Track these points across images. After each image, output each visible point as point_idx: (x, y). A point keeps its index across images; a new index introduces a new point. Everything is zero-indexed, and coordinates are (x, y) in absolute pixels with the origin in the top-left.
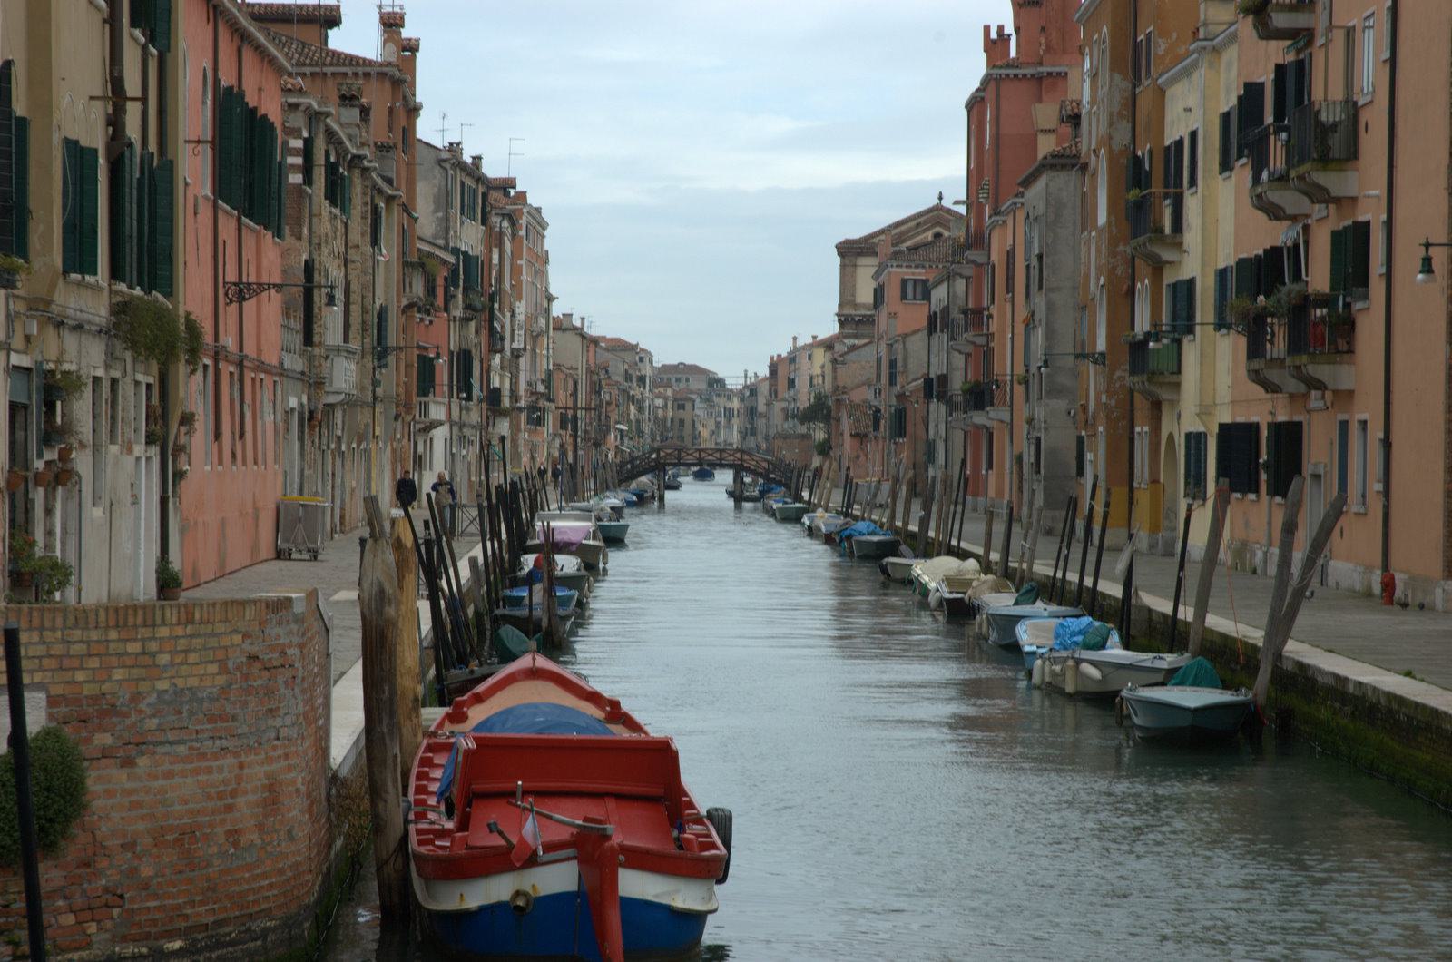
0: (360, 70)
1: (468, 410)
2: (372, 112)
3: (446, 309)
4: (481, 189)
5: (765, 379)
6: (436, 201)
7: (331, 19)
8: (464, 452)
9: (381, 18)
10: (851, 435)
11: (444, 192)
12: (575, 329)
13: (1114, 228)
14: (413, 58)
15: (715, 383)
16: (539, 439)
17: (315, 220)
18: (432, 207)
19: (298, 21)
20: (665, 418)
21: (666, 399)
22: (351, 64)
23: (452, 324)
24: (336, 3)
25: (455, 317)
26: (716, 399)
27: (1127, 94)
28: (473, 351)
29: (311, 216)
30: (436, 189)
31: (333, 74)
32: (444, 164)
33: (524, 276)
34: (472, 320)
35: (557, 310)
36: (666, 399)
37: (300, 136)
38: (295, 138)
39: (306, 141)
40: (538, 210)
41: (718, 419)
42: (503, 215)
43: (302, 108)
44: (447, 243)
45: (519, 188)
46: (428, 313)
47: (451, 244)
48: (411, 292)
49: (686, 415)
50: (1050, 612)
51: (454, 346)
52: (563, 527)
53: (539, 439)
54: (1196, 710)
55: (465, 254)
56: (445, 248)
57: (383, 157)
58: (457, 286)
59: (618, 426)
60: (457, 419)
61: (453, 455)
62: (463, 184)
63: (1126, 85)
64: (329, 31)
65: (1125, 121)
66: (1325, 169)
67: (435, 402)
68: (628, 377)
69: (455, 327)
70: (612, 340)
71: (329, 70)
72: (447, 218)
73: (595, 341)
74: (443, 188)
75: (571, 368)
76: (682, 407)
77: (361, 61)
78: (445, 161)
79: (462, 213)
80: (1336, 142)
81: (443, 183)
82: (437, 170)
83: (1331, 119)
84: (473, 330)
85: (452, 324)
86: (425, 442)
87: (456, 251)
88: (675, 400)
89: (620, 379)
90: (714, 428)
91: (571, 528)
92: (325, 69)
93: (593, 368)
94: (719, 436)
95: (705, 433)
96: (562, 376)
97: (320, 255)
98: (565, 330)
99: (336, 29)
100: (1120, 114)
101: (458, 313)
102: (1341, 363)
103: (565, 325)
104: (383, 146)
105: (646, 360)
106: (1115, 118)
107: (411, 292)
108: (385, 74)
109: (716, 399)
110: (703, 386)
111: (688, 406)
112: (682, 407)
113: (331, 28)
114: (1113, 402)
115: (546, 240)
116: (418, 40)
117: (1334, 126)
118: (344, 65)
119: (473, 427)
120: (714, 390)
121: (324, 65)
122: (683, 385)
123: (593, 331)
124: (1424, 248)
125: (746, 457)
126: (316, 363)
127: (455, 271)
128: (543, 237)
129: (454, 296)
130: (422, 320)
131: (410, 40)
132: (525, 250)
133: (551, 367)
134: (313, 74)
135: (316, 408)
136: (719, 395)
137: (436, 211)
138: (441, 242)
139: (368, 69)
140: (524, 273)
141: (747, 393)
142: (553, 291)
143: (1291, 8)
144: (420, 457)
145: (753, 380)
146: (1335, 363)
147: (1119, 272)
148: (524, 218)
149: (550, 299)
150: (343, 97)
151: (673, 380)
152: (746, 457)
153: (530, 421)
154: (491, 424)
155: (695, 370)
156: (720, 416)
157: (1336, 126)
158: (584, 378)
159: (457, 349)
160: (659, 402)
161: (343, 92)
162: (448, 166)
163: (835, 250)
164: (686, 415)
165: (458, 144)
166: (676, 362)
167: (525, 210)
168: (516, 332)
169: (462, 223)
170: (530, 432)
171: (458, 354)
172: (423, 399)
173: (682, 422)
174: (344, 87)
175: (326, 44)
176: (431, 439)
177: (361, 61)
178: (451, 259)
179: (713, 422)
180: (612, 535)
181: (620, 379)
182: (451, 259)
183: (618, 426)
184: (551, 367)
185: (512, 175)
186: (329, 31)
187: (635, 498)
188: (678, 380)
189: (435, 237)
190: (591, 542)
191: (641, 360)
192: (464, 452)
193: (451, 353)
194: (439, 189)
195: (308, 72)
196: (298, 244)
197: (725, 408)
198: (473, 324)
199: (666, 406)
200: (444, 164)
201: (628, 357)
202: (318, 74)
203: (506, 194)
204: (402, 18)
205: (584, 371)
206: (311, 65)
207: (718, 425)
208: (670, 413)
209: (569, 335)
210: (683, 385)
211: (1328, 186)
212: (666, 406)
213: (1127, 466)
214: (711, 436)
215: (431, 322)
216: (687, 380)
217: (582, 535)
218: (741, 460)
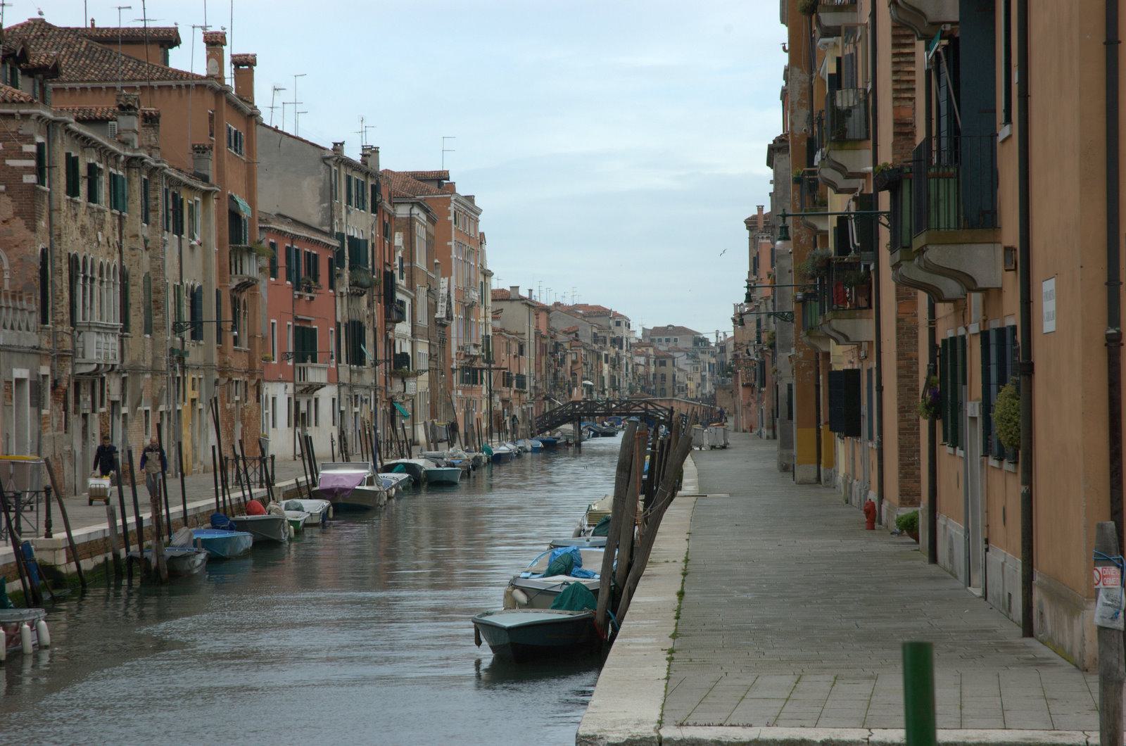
0: (183, 83)
1: (360, 373)
2: (161, 120)
3: (332, 286)
4: (370, 182)
5: (731, 338)
6: (322, 194)
7: (169, 39)
8: (357, 409)
9: (205, 37)
10: (743, 385)
11: (328, 185)
12: (522, 299)
13: (798, 203)
14: (251, 72)
15: (700, 341)
16: (475, 395)
17: (55, 214)
18: (318, 199)
19: (122, 42)
20: (648, 374)
21: (648, 357)
22: (176, 79)
23: (338, 300)
24: (174, 26)
25: (342, 293)
26: (701, 356)
27: (806, 85)
28: (366, 322)
29: (51, 211)
30: (322, 184)
31: (159, 87)
32: (327, 162)
33: (454, 255)
34: (362, 295)
35: (495, 284)
36: (648, 357)
37: (32, 142)
38: (28, 144)
39: (40, 146)
40: (470, 199)
41: (704, 373)
42: (413, 204)
43: (33, 117)
44: (332, 229)
45: (451, 180)
46: (309, 290)
47: (336, 230)
48: (241, 273)
49: (668, 370)
50: (592, 543)
51: (343, 318)
52: (341, 475)
53: (475, 395)
54: (510, 630)
55: (351, 238)
56: (330, 234)
57: (199, 158)
58: (342, 266)
59: (585, 382)
60: (347, 381)
61: (342, 412)
62: (349, 179)
63: (806, 77)
64: (170, 50)
65: (804, 109)
66: (841, 149)
67: (313, 367)
68: (596, 338)
69: (342, 302)
70: (592, 307)
71: (155, 84)
72: (331, 208)
73: (546, 310)
74: (328, 181)
75: (517, 334)
76: (663, 364)
77: (185, 76)
78: (328, 158)
79: (349, 202)
80: (854, 125)
81: (328, 178)
82: (322, 166)
83: (845, 105)
84: (366, 303)
85: (338, 300)
86: (309, 402)
87: (340, 236)
88: (657, 358)
89: (588, 341)
90: (700, 381)
91: (349, 476)
92: (152, 83)
93: (544, 333)
94: (704, 387)
95: (692, 386)
96: (504, 341)
97: (60, 245)
98: (513, 300)
99: (176, 48)
100: (800, 104)
101: (345, 289)
102: (861, 318)
103: (513, 297)
104: (199, 148)
105: (623, 324)
106: (796, 106)
107: (241, 273)
108: (204, 86)
109: (701, 356)
110: (690, 345)
111: (669, 362)
112: (663, 364)
113: (171, 48)
114: (801, 354)
115: (480, 223)
116: (254, 55)
117: (849, 111)
118: (170, 79)
119: (367, 387)
120: (700, 349)
121: (152, 79)
122: (671, 344)
123: (547, 300)
124: (781, 218)
125: (650, 407)
126: (59, 339)
127: (339, 253)
128: (477, 221)
129: (339, 275)
130: (300, 296)
131: (247, 55)
132: (453, 232)
133: (490, 333)
134: (142, 88)
135: (60, 378)
136: (703, 352)
137: (322, 202)
138: (327, 229)
139: (189, 82)
140: (453, 252)
141: (718, 350)
142: (489, 267)
143: (840, 8)
144: (303, 415)
145: (722, 339)
146: (855, 318)
147: (803, 240)
148: (452, 205)
149: (487, 274)
150: (121, 107)
151: (664, 341)
152: (650, 407)
153: (464, 380)
154: (389, 384)
155: (682, 331)
156: (705, 371)
157: (850, 111)
158: (533, 341)
159: (346, 320)
160: (642, 360)
161: (121, 103)
162: (331, 163)
163: (744, 226)
164: (668, 370)
165: (342, 144)
166: (665, 325)
167: (453, 198)
168: (440, 304)
169: (348, 212)
170: (464, 390)
171: (347, 326)
172: (302, 365)
173: (664, 377)
174: (122, 99)
175: (168, 65)
176: (316, 400)
177: (185, 76)
178: (336, 243)
179: (698, 375)
180: (445, 479)
181: (588, 341)
182: (336, 243)
183: (585, 382)
184: (490, 333)
185: (445, 169)
186: (170, 50)
187: (541, 445)
188: (668, 340)
189: (322, 224)
190: (366, 488)
191: (618, 324)
192: (357, 409)
193: (338, 325)
194: (324, 184)
195: (156, 86)
196: (32, 236)
197: (709, 363)
198: (365, 299)
199: (648, 363)
200: (327, 162)
201: (602, 321)
202: (145, 87)
203: (440, 185)
204: (223, 37)
205: (533, 337)
206: (141, 80)
207: (703, 378)
208: (653, 369)
209: (516, 305)
210: (671, 344)
211: (845, 163)
212: (648, 363)
213: (814, 406)
214: (697, 388)
215: (312, 298)
216: (676, 340)
217: (358, 481)
218: (646, 409)
